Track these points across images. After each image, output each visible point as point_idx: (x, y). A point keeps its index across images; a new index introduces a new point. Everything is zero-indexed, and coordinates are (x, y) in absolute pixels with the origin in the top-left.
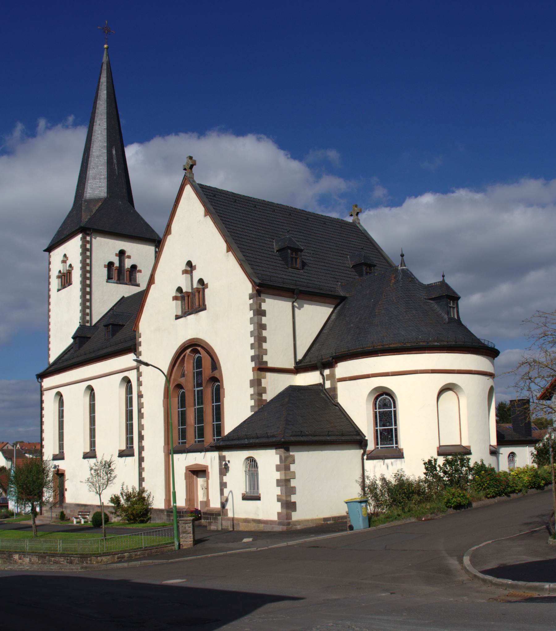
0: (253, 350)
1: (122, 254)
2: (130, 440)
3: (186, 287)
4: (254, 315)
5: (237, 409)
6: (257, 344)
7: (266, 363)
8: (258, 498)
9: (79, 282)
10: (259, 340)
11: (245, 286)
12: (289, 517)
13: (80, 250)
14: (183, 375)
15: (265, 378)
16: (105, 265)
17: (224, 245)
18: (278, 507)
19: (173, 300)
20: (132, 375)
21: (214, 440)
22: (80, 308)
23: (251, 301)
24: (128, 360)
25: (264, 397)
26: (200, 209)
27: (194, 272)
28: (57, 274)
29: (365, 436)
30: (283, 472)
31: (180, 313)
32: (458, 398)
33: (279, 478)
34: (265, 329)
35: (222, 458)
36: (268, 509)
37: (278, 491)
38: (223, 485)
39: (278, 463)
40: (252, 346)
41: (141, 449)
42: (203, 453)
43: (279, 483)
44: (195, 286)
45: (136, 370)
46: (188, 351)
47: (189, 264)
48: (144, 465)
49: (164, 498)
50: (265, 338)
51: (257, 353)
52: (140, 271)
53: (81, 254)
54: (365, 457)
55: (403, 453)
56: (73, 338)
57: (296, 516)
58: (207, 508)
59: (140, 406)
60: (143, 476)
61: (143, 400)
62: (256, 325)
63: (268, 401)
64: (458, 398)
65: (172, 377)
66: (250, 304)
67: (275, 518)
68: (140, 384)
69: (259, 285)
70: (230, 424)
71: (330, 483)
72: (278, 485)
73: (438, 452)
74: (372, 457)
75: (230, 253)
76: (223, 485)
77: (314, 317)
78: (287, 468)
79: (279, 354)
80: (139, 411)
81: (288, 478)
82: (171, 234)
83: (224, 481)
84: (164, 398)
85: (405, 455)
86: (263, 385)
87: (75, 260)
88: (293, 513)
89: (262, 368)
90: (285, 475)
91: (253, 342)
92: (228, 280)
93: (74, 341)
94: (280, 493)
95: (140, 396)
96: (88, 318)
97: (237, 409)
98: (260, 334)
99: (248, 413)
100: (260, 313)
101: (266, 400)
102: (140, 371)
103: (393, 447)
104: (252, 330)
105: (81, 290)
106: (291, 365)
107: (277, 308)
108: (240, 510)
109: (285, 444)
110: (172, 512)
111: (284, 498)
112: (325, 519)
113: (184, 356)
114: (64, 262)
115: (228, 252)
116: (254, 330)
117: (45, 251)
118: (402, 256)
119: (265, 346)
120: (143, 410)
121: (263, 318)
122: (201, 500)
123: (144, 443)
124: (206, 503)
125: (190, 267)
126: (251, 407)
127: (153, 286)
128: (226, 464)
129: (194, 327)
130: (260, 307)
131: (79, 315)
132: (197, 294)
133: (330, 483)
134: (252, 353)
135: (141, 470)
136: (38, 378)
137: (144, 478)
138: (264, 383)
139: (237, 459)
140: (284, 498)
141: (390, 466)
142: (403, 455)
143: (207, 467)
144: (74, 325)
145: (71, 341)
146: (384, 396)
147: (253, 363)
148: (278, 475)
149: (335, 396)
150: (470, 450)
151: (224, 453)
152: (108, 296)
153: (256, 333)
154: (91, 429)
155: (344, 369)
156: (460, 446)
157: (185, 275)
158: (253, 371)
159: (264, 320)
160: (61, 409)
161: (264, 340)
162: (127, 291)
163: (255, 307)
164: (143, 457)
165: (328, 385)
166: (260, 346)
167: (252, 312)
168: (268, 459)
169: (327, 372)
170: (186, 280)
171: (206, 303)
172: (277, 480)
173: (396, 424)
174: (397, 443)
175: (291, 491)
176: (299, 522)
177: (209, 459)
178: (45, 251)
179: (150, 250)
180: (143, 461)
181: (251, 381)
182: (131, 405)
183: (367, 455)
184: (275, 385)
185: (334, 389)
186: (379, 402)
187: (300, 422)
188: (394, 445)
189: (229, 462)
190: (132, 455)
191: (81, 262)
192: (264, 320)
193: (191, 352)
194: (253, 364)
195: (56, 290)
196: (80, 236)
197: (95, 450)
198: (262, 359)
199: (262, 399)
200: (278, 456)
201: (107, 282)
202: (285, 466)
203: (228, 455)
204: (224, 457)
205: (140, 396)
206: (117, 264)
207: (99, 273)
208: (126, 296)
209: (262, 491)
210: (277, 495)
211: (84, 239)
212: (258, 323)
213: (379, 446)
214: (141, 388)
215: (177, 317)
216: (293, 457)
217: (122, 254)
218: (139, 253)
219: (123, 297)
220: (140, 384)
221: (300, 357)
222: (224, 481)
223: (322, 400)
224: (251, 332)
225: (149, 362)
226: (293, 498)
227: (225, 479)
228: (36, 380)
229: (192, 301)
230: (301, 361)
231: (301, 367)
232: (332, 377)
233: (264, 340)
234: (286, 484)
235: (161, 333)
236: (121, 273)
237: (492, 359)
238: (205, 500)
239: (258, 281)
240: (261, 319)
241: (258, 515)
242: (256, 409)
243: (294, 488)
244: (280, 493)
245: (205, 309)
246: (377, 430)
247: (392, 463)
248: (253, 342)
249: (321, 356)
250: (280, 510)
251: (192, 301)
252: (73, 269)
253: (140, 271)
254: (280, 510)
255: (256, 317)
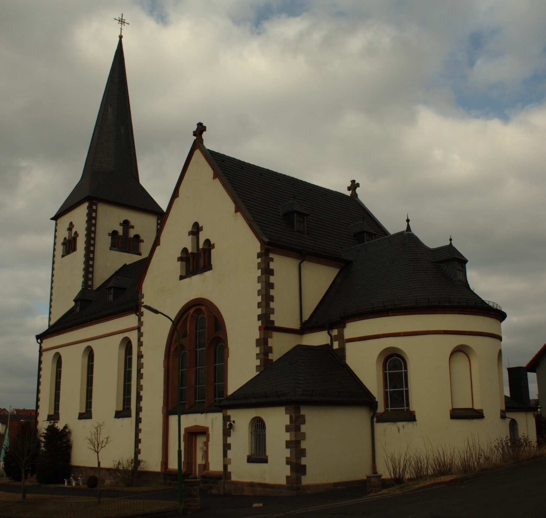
0: (260, 309)
1: (126, 224)
2: (127, 401)
3: (192, 249)
4: (262, 273)
5: (241, 368)
6: (264, 303)
7: (273, 322)
8: (265, 460)
9: (84, 249)
10: (266, 298)
11: (253, 245)
12: (299, 480)
13: (86, 218)
14: (185, 336)
15: (271, 337)
16: (109, 233)
17: (231, 206)
18: (287, 470)
19: (178, 261)
20: (133, 336)
21: (216, 401)
22: (83, 273)
23: (259, 260)
24: (131, 320)
25: (270, 356)
26: (210, 172)
27: (201, 233)
28: (62, 241)
29: (375, 398)
30: (294, 433)
31: (184, 274)
32: (469, 360)
33: (288, 439)
34: (273, 288)
35: (226, 419)
36: (275, 471)
37: (287, 453)
38: (227, 447)
39: (288, 423)
40: (259, 305)
41: (139, 409)
42: (204, 415)
43: (288, 444)
44: (201, 246)
45: (136, 331)
46: (192, 311)
47: (196, 225)
48: (141, 426)
49: (161, 460)
50: (273, 297)
51: (264, 312)
52: (143, 241)
53: (87, 222)
54: (375, 420)
55: (415, 416)
56: (74, 301)
57: (306, 480)
58: (206, 471)
59: (140, 366)
60: (140, 437)
61: (143, 360)
62: (264, 284)
63: (274, 360)
64: (469, 360)
65: (174, 338)
66: (258, 263)
67: (283, 482)
68: (140, 344)
69: (268, 244)
70: (234, 384)
71: (337, 445)
72: (287, 447)
73: (451, 415)
74: (383, 418)
75: (239, 213)
76: (227, 447)
77: (319, 279)
78: (298, 429)
79: (286, 315)
80: (139, 371)
81: (298, 439)
82: (178, 196)
83: (228, 442)
84: (165, 358)
85: (417, 418)
86: (269, 345)
87: (81, 228)
88: (303, 478)
89: (268, 326)
90: (296, 436)
91: (260, 301)
92: (236, 242)
93: (76, 304)
94: (289, 456)
95: (140, 356)
96: (90, 283)
97: (241, 368)
98: (268, 292)
99: (254, 373)
100: (267, 272)
101: (272, 360)
102: (142, 331)
103: (404, 409)
104: (260, 288)
105: (85, 263)
106: (295, 325)
107: (284, 267)
108: (243, 472)
109: (294, 404)
110: (166, 474)
111: (294, 461)
112: (335, 484)
113: (187, 316)
114: (70, 229)
115: (236, 212)
116: (262, 288)
117: (52, 219)
118: (408, 221)
119: (272, 305)
120: (142, 371)
121: (271, 277)
122: (200, 463)
123: (142, 404)
124: (206, 466)
125: (196, 230)
126: (257, 366)
127: (158, 248)
128: (231, 425)
129: (198, 287)
130: (268, 266)
131: (82, 279)
132: (202, 255)
133: (337, 445)
134: (259, 311)
135: (138, 431)
136: (37, 339)
137: (140, 440)
138: (270, 342)
139: (242, 419)
140: (294, 461)
141: (401, 428)
142: (415, 416)
143: (207, 429)
144: (78, 287)
145: (73, 304)
146: (395, 357)
147: (260, 322)
148: (287, 436)
149: (344, 357)
150: (483, 414)
151: (230, 412)
152: (110, 262)
153: (264, 292)
154: (87, 390)
155: (353, 329)
156: (472, 409)
157: (191, 236)
158: (259, 330)
159: (272, 279)
160: (59, 369)
161: (272, 299)
162: (129, 259)
163: (263, 266)
164: (141, 418)
165: (336, 345)
166: (268, 305)
167: (260, 271)
168: (276, 420)
169: (335, 332)
170: (192, 241)
171: (212, 263)
172: (287, 442)
173: (407, 386)
174: (408, 405)
175: (302, 453)
176: (309, 487)
177: (213, 421)
178: (52, 219)
179: (151, 222)
180: (140, 422)
181: (257, 340)
182: (130, 366)
183: (377, 417)
184: (281, 345)
185: (342, 350)
186: (389, 363)
187: (309, 380)
188: (405, 408)
189: (234, 422)
190: (129, 416)
191: (87, 229)
192: (272, 279)
193: (194, 312)
194: (260, 324)
195: (61, 256)
196: (86, 205)
197: (91, 411)
198: (269, 318)
199: (268, 359)
200: (288, 416)
201: (110, 249)
202: (295, 425)
203: (233, 414)
204: (229, 417)
205: (140, 356)
206: (121, 233)
207: (103, 241)
208: (127, 264)
209: (270, 452)
210: (287, 458)
211: (90, 208)
212: (266, 282)
213: (389, 409)
214: (142, 349)
215: (182, 278)
216: (303, 417)
217: (126, 224)
218: (143, 225)
219: (125, 264)
220: (140, 344)
221: (306, 317)
222: (228, 442)
223: (332, 360)
224: (259, 291)
225: (160, 311)
226: (304, 461)
227: (229, 440)
228: (36, 340)
229: (197, 261)
230: (307, 322)
231: (307, 327)
232: (340, 338)
233: (272, 299)
234: (296, 446)
235: (166, 291)
236: (124, 241)
237: (499, 322)
238: (204, 463)
239: (266, 240)
240: (269, 278)
241: (264, 479)
242: (262, 369)
243: (305, 449)
244: (289, 456)
245: (211, 269)
246: (387, 392)
247: (403, 426)
248: (260, 301)
249: (331, 314)
250: (289, 474)
251: (197, 261)
252: (78, 236)
253: (143, 241)
254: (289, 474)
255: (264, 276)
